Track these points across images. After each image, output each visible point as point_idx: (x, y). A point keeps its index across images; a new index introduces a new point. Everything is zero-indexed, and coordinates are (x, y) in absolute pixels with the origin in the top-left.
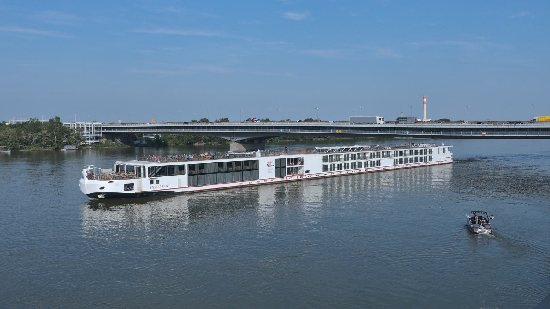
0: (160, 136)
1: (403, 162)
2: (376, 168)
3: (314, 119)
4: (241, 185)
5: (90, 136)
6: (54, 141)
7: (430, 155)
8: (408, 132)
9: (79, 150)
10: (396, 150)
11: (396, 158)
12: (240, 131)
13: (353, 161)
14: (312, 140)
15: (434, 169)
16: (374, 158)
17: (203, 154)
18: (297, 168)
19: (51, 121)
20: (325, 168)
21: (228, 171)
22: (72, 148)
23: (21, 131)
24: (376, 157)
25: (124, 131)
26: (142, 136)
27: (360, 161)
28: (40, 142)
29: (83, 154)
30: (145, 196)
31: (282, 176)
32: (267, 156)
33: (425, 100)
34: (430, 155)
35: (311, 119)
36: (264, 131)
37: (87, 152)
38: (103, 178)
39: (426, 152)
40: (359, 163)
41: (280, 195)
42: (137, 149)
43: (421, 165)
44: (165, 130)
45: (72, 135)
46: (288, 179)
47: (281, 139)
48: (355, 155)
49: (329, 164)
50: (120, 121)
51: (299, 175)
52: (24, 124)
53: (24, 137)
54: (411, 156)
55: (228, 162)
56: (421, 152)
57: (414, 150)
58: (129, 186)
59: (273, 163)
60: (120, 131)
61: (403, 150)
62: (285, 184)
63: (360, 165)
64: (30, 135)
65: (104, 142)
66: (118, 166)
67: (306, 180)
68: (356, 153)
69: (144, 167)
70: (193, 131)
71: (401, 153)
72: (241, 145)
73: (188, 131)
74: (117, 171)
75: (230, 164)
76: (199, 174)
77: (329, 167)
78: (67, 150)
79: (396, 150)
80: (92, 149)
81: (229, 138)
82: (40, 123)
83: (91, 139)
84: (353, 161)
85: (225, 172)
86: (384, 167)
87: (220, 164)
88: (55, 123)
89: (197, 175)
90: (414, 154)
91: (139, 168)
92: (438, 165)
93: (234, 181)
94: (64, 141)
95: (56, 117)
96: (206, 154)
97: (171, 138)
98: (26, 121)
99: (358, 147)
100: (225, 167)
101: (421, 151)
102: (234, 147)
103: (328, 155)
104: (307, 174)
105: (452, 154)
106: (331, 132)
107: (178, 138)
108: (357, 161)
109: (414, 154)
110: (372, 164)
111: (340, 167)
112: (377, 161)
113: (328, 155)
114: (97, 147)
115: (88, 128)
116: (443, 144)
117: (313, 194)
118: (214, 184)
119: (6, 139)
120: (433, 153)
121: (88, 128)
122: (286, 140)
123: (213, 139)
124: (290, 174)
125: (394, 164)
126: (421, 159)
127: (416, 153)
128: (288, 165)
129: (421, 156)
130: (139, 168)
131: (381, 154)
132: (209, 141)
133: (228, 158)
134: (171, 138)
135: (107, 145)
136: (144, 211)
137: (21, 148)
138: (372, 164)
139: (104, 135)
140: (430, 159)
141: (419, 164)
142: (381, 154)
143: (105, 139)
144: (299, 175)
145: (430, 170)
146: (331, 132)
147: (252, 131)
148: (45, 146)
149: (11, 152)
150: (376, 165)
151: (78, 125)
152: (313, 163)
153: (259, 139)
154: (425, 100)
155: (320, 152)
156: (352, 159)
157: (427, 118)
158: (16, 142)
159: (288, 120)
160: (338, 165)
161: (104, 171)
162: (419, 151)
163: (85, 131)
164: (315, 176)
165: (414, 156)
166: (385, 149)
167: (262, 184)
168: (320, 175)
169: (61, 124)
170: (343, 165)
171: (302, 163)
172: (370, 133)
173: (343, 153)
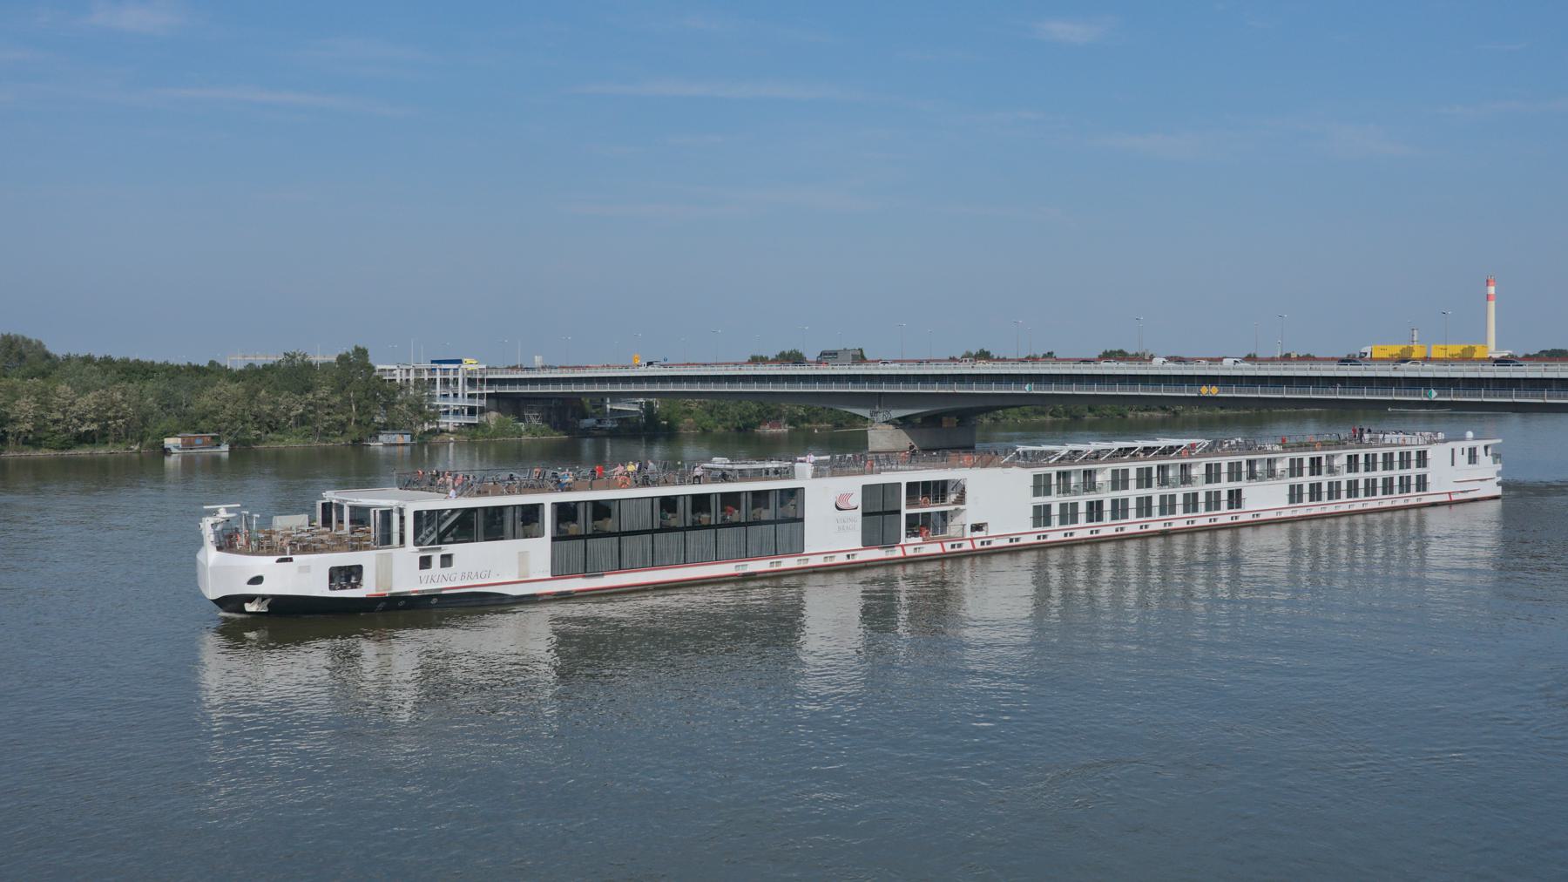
0: (657, 405)
1: (1325, 496)
2: (1224, 516)
3: (1131, 352)
4: (741, 571)
5: (452, 404)
6: (349, 420)
7: (1421, 471)
8: (1434, 393)
9: (421, 445)
10: (1296, 455)
11: (1296, 480)
12: (884, 389)
13: (1144, 492)
14: (1125, 417)
15: (1432, 516)
16: (1218, 480)
17: (620, 469)
18: (944, 514)
19: (341, 359)
20: (1042, 516)
21: (697, 526)
22: (399, 439)
23: (258, 391)
24: (1224, 477)
25: (550, 389)
26: (602, 406)
27: (1167, 491)
28: (311, 422)
29: (431, 458)
30: (403, 608)
31: (888, 541)
32: (832, 475)
33: (1492, 290)
34: (1421, 471)
35: (1121, 352)
36: (975, 389)
37: (442, 453)
38: (264, 547)
39: (1405, 461)
40: (1163, 498)
41: (878, 613)
42: (587, 446)
43: (1387, 504)
44: (671, 388)
45: (401, 403)
46: (910, 552)
47: (1025, 415)
48: (1149, 470)
49: (1055, 501)
50: (538, 361)
51: (950, 539)
52: (267, 368)
53: (267, 408)
54: (1352, 476)
55: (694, 497)
56: (1388, 462)
57: (1224, 463)
58: (346, 575)
59: (857, 500)
60: (539, 389)
61: (1323, 454)
62: (899, 571)
63: (1168, 505)
64: (284, 400)
65: (492, 423)
66: (327, 508)
67: (972, 554)
68: (1154, 464)
69: (401, 511)
70: (755, 388)
71: (1316, 465)
72: (902, 433)
73: (740, 388)
74: (327, 521)
75: (700, 502)
76: (720, 526)
77: (1055, 510)
78: (386, 445)
79: (1296, 455)
80: (456, 442)
81: (865, 413)
82: (310, 366)
83: (456, 413)
84: (1144, 492)
85: (685, 529)
86: (1256, 513)
87: (668, 503)
88: (355, 365)
89: (585, 537)
90: (1362, 467)
91: (386, 515)
92: (1450, 503)
93: (718, 560)
94: (377, 419)
95: (357, 349)
96: (632, 468)
97: (689, 412)
98: (271, 359)
99: (1163, 443)
100: (683, 516)
101: (1388, 458)
102: (882, 437)
103: (1053, 471)
104: (977, 534)
105: (1499, 467)
106: (1186, 392)
107: (711, 412)
108: (1155, 492)
109: (1362, 467)
110: (1213, 501)
111: (1095, 510)
112: (1230, 493)
113: (1053, 471)
114: (472, 436)
115: (446, 382)
116: (1470, 434)
117: (997, 605)
118: (644, 567)
119: (216, 413)
120: (1429, 463)
121: (446, 382)
122: (1042, 418)
123: (649, 422)
124: (916, 535)
125: (1292, 501)
126: (1388, 486)
127: (1370, 464)
128: (908, 505)
129: (1388, 474)
130: (386, 515)
131: (1244, 467)
132: (803, 420)
133: (697, 480)
134: (689, 412)
135: (502, 430)
136: (396, 660)
137: (258, 440)
138: (1213, 501)
139: (493, 402)
140: (1422, 483)
141: (1380, 501)
142: (1244, 467)
143: (494, 414)
144: (950, 539)
145: (1421, 523)
146: (1186, 392)
147: (936, 389)
148: (325, 434)
149: (230, 451)
150: (1224, 505)
151: (418, 371)
152: (997, 496)
153: (821, 414)
154: (1492, 290)
155: (1029, 460)
156: (1139, 486)
157: (1498, 348)
158: (244, 422)
159: (1049, 356)
160: (1090, 505)
161: (282, 522)
162: (1380, 459)
163: (438, 390)
164: (1005, 542)
165: (1361, 476)
166: (1262, 450)
167: (816, 570)
168: (1025, 540)
169: (372, 368)
170: (1107, 506)
171: (961, 499)
172: (1311, 394)
173: (1106, 465)
